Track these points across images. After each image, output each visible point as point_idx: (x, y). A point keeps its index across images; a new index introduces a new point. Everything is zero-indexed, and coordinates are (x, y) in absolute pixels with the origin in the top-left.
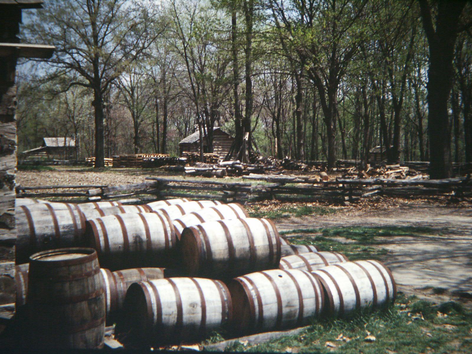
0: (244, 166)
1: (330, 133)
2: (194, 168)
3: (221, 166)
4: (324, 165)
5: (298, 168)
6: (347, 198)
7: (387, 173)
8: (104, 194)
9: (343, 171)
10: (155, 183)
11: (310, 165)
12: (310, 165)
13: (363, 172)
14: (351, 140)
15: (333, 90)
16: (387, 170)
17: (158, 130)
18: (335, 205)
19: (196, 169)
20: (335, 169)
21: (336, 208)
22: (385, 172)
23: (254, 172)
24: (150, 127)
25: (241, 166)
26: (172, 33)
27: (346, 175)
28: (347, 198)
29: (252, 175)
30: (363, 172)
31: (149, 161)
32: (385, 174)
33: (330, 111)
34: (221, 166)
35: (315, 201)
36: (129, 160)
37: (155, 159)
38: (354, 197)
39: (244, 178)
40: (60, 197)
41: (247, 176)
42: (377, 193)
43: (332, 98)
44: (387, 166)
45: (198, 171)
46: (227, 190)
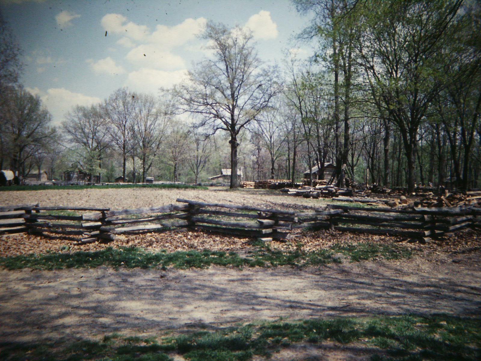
0: (336, 189)
1: (410, 163)
2: (295, 190)
3: (317, 189)
4: (405, 190)
5: (384, 192)
6: (427, 233)
7: (468, 199)
8: (106, 220)
9: (421, 195)
10: (186, 207)
11: (393, 190)
12: (393, 190)
13: (443, 197)
14: (428, 173)
15: (413, 131)
16: (468, 196)
17: (289, 165)
18: (410, 242)
19: (297, 190)
20: (414, 194)
21: (412, 245)
22: (465, 198)
23: (343, 194)
24: (285, 162)
25: (333, 189)
26: (425, 201)
27: (424, 200)
28: (427, 233)
29: (341, 197)
30: (443, 197)
31: (275, 185)
32: (466, 200)
33: (410, 148)
34: (317, 189)
35: (385, 235)
36: (264, 184)
37: (279, 183)
38: (437, 232)
39: (333, 199)
40: (222, 210)
41: (337, 198)
42: (468, 226)
43: (413, 137)
44: (468, 193)
45: (298, 192)
46: (265, 218)
